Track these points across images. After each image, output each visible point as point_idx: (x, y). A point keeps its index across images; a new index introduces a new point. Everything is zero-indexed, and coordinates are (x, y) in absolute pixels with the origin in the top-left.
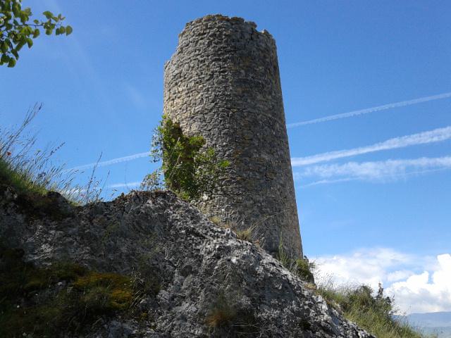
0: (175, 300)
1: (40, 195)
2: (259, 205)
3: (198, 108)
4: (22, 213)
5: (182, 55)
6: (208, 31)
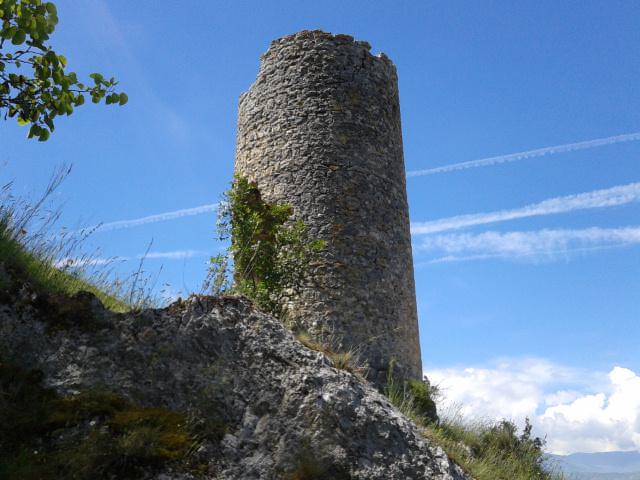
0: (249, 447)
1: (67, 295)
3: (285, 163)
4: (43, 321)
5: (264, 86)
6: (302, 53)
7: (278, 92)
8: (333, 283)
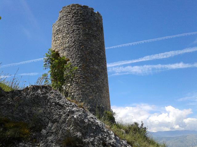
0: (49, 134)
2: (92, 88)
3: (67, 45)
7: (65, 23)
8: (82, 82)
